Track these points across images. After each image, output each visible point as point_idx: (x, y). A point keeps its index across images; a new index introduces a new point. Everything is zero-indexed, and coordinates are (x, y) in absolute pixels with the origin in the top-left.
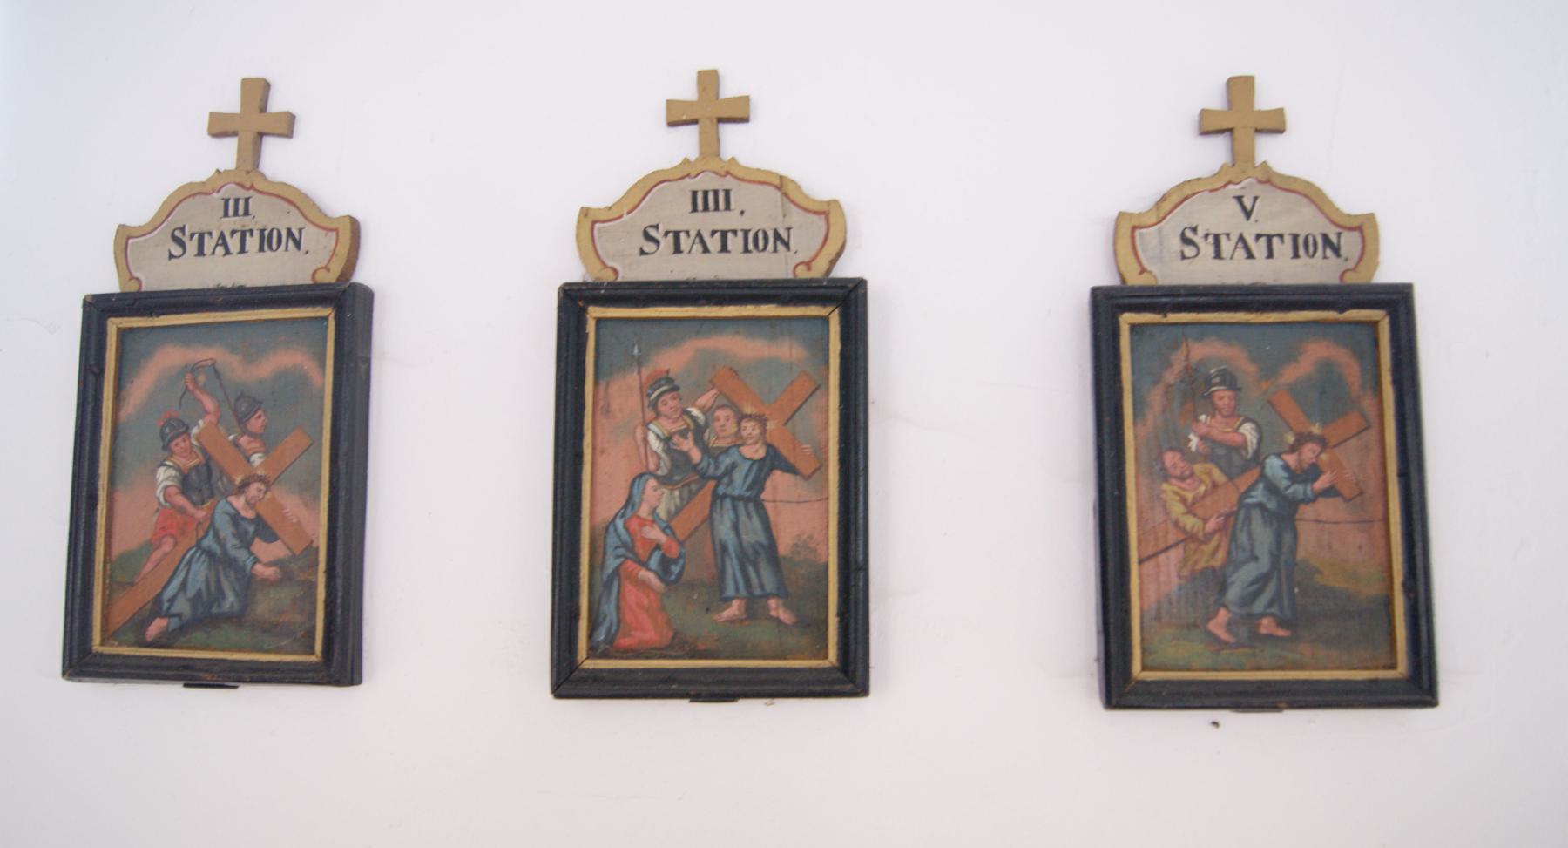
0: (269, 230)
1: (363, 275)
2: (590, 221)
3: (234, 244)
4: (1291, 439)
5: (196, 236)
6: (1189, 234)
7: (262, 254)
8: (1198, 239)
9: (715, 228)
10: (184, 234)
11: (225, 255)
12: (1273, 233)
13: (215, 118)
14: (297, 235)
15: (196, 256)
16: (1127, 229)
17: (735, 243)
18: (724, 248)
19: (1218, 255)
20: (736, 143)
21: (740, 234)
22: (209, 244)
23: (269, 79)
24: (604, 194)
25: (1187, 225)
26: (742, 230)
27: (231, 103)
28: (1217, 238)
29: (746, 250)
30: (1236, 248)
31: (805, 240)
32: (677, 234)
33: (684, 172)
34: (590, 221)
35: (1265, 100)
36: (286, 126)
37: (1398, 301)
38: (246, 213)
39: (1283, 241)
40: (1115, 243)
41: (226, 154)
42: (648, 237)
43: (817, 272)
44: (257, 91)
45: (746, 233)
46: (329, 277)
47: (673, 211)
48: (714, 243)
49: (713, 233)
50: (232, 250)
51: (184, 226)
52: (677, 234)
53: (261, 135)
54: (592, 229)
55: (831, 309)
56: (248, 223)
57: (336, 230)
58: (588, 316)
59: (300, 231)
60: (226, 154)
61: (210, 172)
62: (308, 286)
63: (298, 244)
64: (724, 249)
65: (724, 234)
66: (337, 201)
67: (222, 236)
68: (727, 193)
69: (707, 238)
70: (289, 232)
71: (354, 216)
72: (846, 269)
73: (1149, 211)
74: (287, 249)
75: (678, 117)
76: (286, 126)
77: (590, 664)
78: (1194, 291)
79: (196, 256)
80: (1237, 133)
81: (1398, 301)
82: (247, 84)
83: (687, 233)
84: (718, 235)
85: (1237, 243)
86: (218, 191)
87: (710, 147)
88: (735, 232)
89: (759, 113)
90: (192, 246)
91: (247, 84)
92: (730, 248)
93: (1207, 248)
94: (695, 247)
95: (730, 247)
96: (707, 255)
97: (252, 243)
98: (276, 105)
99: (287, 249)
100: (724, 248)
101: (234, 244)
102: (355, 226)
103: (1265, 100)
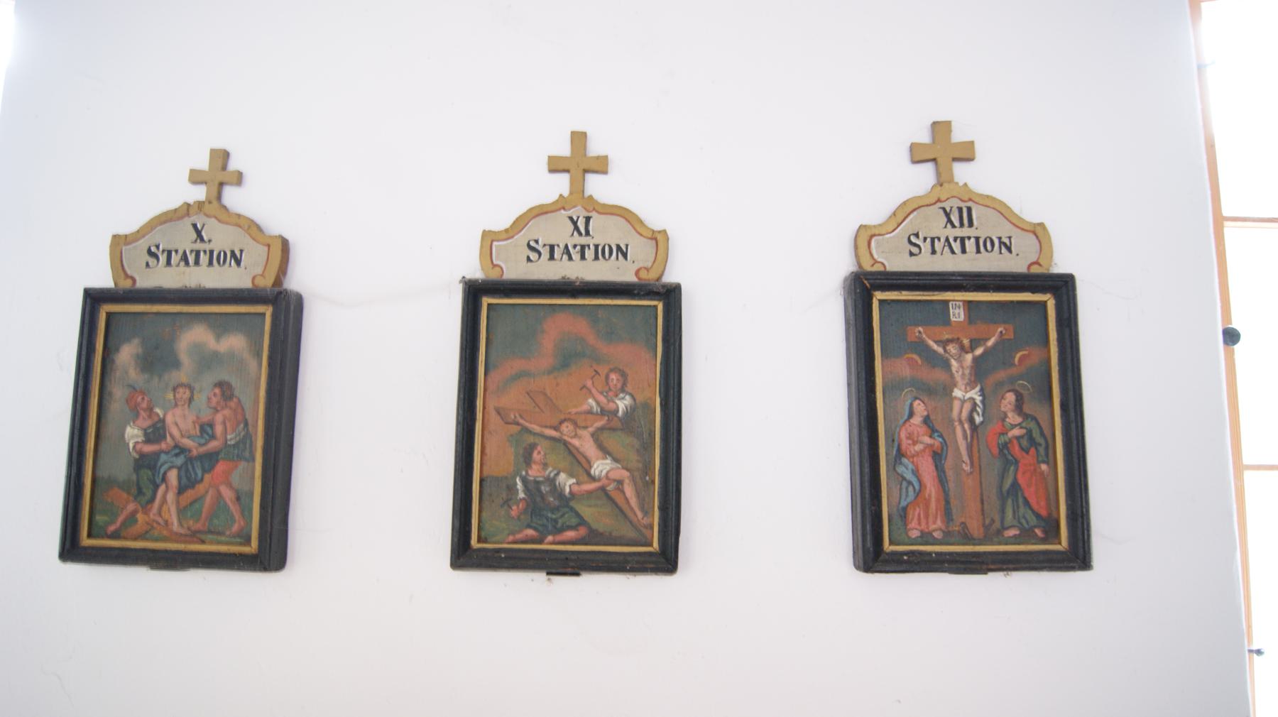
1: (297, 281)
2: (489, 238)
3: (191, 259)
4: (171, 396)
5: (929, 240)
6: (913, 239)
9: (957, 235)
13: (552, 160)
16: (865, 237)
19: (934, 252)
20: (597, 187)
21: (973, 240)
22: (175, 258)
23: (229, 149)
24: (129, 225)
25: (607, 243)
26: (974, 237)
27: (203, 163)
28: (933, 240)
30: (944, 246)
31: (640, 253)
32: (169, 253)
33: (561, 204)
34: (489, 238)
35: (958, 136)
36: (239, 179)
38: (971, 224)
40: (856, 247)
41: (560, 185)
42: (150, 253)
43: (652, 276)
44: (220, 158)
45: (977, 239)
46: (267, 282)
47: (557, 231)
48: (956, 246)
49: (575, 246)
50: (556, 256)
51: (159, 245)
52: (933, 240)
53: (934, 160)
58: (101, 310)
60: (560, 185)
61: (555, 197)
62: (248, 290)
63: (238, 262)
64: (964, 251)
65: (963, 240)
66: (275, 224)
68: (969, 209)
69: (951, 240)
71: (286, 236)
73: (649, 228)
74: (617, 258)
75: (556, 166)
76: (239, 179)
80: (939, 160)
81: (1063, 287)
82: (214, 153)
83: (558, 246)
84: (958, 240)
88: (969, 238)
89: (248, 179)
90: (163, 258)
91: (214, 153)
95: (586, 256)
96: (584, 262)
97: (589, 254)
98: (233, 165)
99: (617, 258)
101: (191, 259)
102: (285, 245)
103: (958, 136)
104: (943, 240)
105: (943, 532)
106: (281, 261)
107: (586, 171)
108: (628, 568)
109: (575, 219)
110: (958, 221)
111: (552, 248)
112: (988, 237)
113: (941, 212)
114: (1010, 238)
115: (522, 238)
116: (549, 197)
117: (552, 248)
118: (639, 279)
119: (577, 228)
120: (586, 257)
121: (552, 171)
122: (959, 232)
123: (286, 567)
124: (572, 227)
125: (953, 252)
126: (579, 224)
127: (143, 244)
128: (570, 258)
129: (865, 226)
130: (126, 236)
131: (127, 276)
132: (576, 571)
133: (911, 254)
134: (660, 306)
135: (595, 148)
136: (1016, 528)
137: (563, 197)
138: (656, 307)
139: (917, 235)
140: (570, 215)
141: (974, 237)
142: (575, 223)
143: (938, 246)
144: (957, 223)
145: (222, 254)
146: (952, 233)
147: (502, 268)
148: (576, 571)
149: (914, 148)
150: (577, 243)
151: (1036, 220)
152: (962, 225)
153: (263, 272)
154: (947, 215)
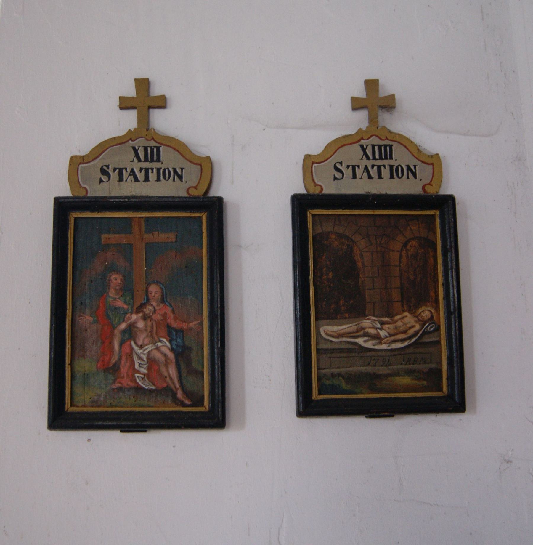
0: (163, 169)
6: (338, 166)
7: (392, 180)
8: (111, 172)
10: (108, 168)
11: (407, 179)
12: (379, 161)
14: (180, 173)
15: (352, 179)
17: (152, 176)
18: (147, 179)
19: (354, 176)
21: (155, 170)
26: (156, 168)
28: (354, 167)
29: (158, 179)
30: (364, 172)
32: (354, 167)
33: (131, 136)
35: (131, 92)
37: (451, 199)
38: (391, 158)
39: (385, 168)
42: (104, 172)
48: (141, 176)
49: (373, 166)
51: (109, 165)
54: (312, 166)
55: (308, 213)
56: (392, 162)
57: (201, 165)
59: (415, 166)
63: (180, 177)
64: (380, 177)
65: (147, 170)
67: (366, 168)
69: (370, 168)
70: (408, 167)
72: (214, 193)
74: (174, 180)
77: (445, 389)
78: (376, 197)
79: (352, 179)
84: (143, 171)
85: (364, 170)
86: (134, 141)
87: (373, 120)
92: (383, 176)
93: (114, 176)
94: (364, 173)
99: (174, 180)
100: (147, 179)
103: (131, 92)
104: (129, 170)
105: (339, 377)
106: (211, 179)
107: (149, 107)
108: (191, 414)
109: (137, 148)
110: (143, 156)
111: (121, 171)
112: (399, 165)
113: (360, 148)
114: (182, 169)
115: (98, 163)
116: (120, 131)
117: (121, 171)
118: (189, 194)
119: (137, 156)
120: (150, 179)
121: (354, 109)
122: (379, 163)
123: (226, 426)
124: (362, 153)
125: (370, 177)
126: (367, 151)
127: (98, 163)
128: (370, 177)
129: (309, 155)
130: (84, 156)
131: (316, 185)
132: (392, 414)
133: (335, 178)
134: (204, 217)
135: (156, 91)
136: (141, 372)
137: (131, 131)
138: (200, 218)
139: (341, 163)
140: (134, 146)
141: (156, 168)
142: (136, 151)
143: (359, 172)
144: (142, 158)
145: (167, 171)
146: (369, 163)
147: (321, 186)
148: (392, 414)
149: (354, 100)
150: (374, 164)
151: (435, 152)
152: (374, 158)
153: (431, 181)
154: (364, 150)
